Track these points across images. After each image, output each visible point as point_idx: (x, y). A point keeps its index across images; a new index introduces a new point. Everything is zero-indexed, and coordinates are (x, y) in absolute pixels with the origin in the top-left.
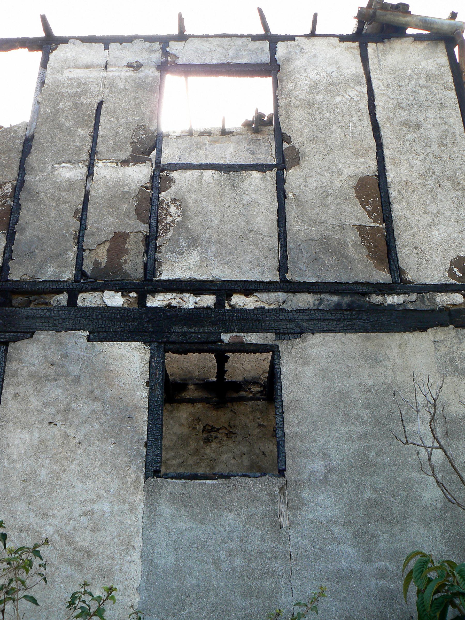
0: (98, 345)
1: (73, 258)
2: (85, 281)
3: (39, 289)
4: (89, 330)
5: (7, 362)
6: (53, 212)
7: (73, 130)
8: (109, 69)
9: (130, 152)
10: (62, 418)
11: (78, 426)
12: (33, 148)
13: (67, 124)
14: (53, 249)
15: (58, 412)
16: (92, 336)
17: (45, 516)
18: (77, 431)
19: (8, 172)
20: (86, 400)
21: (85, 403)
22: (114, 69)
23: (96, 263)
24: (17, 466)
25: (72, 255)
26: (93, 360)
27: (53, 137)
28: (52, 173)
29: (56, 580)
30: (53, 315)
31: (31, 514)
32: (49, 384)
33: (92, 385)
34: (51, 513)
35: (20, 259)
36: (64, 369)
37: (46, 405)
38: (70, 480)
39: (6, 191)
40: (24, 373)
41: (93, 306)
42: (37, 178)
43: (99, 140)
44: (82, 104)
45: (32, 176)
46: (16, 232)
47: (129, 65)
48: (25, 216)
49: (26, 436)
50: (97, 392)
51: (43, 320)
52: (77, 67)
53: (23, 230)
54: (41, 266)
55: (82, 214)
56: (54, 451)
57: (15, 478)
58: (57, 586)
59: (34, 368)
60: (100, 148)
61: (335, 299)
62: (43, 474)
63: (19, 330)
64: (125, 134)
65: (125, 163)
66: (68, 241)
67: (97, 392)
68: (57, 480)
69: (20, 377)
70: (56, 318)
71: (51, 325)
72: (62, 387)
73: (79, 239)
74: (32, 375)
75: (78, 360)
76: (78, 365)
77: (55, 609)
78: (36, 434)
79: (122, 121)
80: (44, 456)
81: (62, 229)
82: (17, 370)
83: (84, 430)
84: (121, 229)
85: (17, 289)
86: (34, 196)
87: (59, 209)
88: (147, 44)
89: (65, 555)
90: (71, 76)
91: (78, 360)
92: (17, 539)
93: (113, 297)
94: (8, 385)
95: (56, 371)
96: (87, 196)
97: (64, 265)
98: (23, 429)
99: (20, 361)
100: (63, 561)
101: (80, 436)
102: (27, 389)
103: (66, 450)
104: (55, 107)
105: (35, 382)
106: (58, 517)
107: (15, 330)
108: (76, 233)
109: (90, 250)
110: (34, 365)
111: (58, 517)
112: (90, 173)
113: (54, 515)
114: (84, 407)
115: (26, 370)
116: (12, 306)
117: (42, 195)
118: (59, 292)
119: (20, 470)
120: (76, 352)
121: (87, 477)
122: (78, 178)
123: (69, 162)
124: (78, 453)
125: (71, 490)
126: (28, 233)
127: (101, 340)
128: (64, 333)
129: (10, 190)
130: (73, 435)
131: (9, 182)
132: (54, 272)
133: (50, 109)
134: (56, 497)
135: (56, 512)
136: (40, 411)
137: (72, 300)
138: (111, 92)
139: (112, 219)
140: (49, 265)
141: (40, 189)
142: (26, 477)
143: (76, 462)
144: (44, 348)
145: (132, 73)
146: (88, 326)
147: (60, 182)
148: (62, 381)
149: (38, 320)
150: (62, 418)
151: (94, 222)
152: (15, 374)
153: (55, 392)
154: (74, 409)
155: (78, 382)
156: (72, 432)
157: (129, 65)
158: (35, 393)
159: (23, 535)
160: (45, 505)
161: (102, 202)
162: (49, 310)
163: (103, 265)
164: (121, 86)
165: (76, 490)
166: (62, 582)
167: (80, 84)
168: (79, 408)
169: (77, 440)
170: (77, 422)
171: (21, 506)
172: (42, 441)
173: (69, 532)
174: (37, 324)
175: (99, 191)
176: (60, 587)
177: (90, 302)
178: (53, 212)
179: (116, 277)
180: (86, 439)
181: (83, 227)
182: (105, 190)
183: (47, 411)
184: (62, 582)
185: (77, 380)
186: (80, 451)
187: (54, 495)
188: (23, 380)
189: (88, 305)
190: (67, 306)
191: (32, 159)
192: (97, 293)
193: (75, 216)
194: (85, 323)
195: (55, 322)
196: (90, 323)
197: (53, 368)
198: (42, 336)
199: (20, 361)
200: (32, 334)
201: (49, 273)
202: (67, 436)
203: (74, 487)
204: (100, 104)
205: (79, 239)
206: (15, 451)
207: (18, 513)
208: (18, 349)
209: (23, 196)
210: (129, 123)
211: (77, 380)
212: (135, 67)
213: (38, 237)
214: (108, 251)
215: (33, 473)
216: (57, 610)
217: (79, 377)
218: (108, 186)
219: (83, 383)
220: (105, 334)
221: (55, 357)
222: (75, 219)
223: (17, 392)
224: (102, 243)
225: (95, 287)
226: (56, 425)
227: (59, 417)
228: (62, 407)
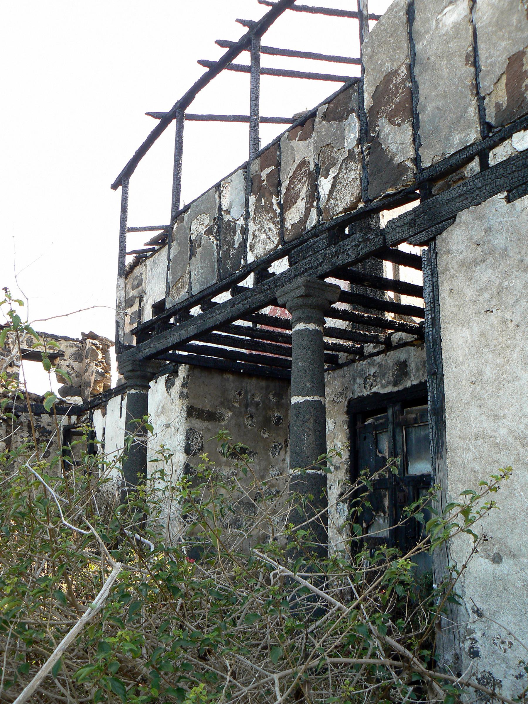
0: (518, 203)
1: (474, 113)
3: (451, 166)
4: (507, 189)
5: (438, 258)
6: (445, 72)
10: (497, 302)
12: (416, 11)
14: (454, 113)
16: (511, 195)
17: (497, 417)
18: (513, 312)
19: (399, 53)
20: (517, 273)
21: (517, 277)
23: (498, 106)
24: (464, 368)
25: (472, 112)
26: (517, 223)
29: (516, 488)
30: (469, 187)
31: (484, 418)
32: (478, 267)
33: (520, 253)
34: (501, 413)
35: (427, 141)
36: (490, 245)
37: (480, 292)
38: (514, 372)
39: (402, 74)
40: (454, 264)
41: (505, 159)
42: (425, 43)
45: (421, 44)
46: (419, 114)
49: (466, 333)
51: (462, 199)
53: (425, 107)
56: (495, 342)
57: (464, 381)
58: (517, 495)
59: (462, 256)
62: (489, 372)
63: (443, 219)
66: (466, 96)
68: (503, 374)
69: (452, 270)
70: (472, 190)
71: (470, 201)
72: (491, 267)
74: (462, 264)
75: (502, 229)
76: (503, 236)
77: (518, 520)
78: (475, 328)
80: (485, 350)
82: (448, 263)
83: (519, 309)
84: (515, 50)
85: (432, 175)
87: (451, 64)
89: (521, 459)
91: (502, 229)
92: (475, 448)
95: (485, 251)
97: (467, 126)
99: (448, 253)
100: (520, 466)
101: (517, 318)
103: (505, 338)
105: (466, 271)
106: (509, 416)
107: (439, 220)
108: (472, 83)
109: (489, 94)
110: (462, 252)
111: (509, 416)
113: (505, 415)
115: (455, 260)
116: (434, 196)
117: (432, 59)
118: (470, 159)
119: (467, 372)
120: (498, 220)
122: (462, 17)
124: (518, 338)
125: (517, 383)
126: (429, 109)
127: (520, 196)
128: (483, 204)
130: (509, 319)
131: (402, 64)
132: (460, 139)
134: (504, 394)
135: (506, 411)
140: (453, 134)
142: (473, 379)
143: (517, 349)
144: (468, 230)
146: (505, 185)
148: (490, 260)
149: (457, 200)
150: (497, 302)
151: (487, 58)
152: (447, 269)
153: (486, 274)
154: (506, 288)
155: (506, 255)
156: (508, 315)
158: (468, 282)
159: (480, 442)
160: (495, 406)
161: (490, 29)
162: (464, 185)
163: (505, 105)
165: (522, 382)
166: (522, 489)
168: (511, 285)
169: (514, 323)
170: (511, 302)
171: (474, 411)
172: (482, 334)
173: (522, 432)
174: (458, 205)
175: (485, 18)
176: (521, 495)
177: (502, 155)
178: (445, 72)
179: (521, 112)
180: (523, 319)
182: (490, 12)
183: (481, 299)
184: (522, 489)
185: (505, 253)
186: (519, 335)
187: (501, 392)
188: (454, 272)
189: (500, 160)
190: (481, 172)
194: (502, 182)
195: (473, 195)
196: (506, 180)
197: (480, 248)
198: (463, 217)
199: (448, 253)
201: (455, 143)
202: (505, 321)
203: (519, 379)
206: (460, 352)
207: (472, 420)
209: (417, 71)
213: (438, 108)
214: (506, 85)
215: (480, 373)
216: (521, 522)
217: (506, 249)
219: (511, 255)
220: (524, 186)
221: (478, 235)
222: (468, 67)
223: (451, 287)
224: (499, 80)
225: (503, 135)
226: (492, 311)
227: (494, 302)
228: (494, 289)
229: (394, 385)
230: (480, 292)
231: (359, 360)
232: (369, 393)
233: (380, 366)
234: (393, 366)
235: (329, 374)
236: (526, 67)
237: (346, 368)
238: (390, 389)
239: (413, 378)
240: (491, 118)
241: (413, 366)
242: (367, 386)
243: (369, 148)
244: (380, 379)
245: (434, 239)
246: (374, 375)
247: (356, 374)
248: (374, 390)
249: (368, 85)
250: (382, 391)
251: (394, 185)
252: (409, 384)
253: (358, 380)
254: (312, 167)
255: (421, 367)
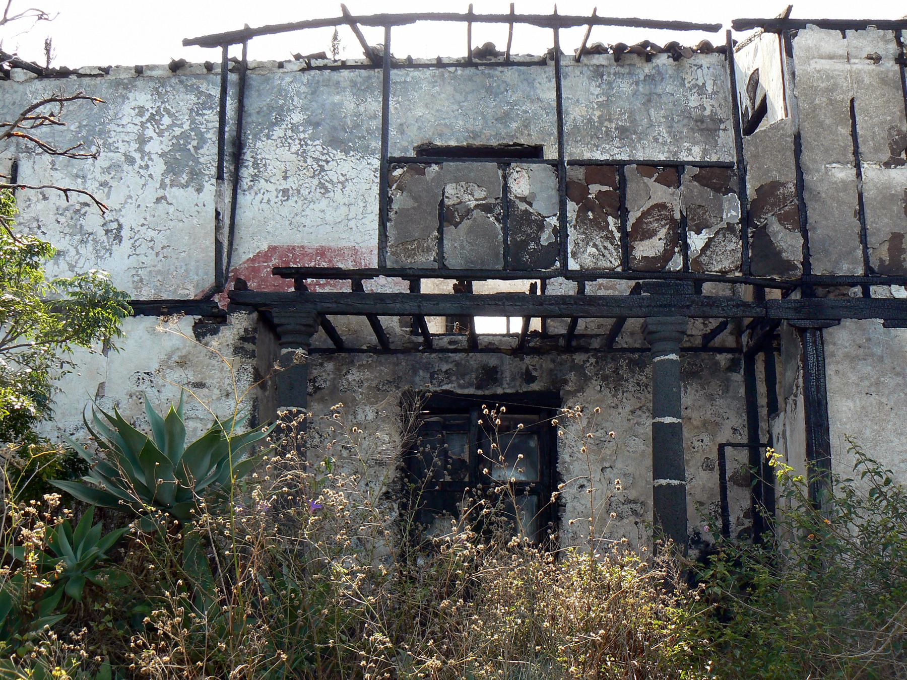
0: (892, 330)
2: (871, 277)
7: (834, 128)
8: (852, 61)
9: (889, 154)
11: (888, 396)
13: (827, 121)
15: (871, 385)
22: (856, 61)
23: (881, 260)
25: (860, 253)
27: (818, 135)
28: (826, 173)
32: (860, 362)
37: (861, 379)
40: (840, 353)
43: (860, 140)
44: (837, 101)
47: (869, 57)
48: (813, 215)
49: (851, 404)
50: (898, 369)
52: (821, 57)
53: (814, 229)
54: (837, 262)
55: (861, 214)
60: (862, 149)
61: (516, 324)
64: (881, 134)
65: (887, 165)
67: (898, 369)
73: (863, 236)
74: (846, 356)
79: (876, 120)
81: (847, 229)
84: (896, 230)
86: (816, 196)
88: (881, 32)
90: (818, 67)
93: (898, 291)
94: (830, 364)
95: (863, 353)
96: (860, 196)
98: (848, 398)
99: (835, 344)
102: (845, 367)
104: (812, 102)
112: (859, 175)
114: (890, 381)
115: (840, 351)
118: (853, 285)
121: (901, 434)
123: (839, 162)
126: (819, 231)
129: (793, 189)
133: (808, 104)
136: (857, 385)
137: (357, 287)
138: (859, 88)
139: (886, 220)
141: (820, 189)
143: (891, 423)
145: (873, 67)
147: (835, 183)
148: (870, 360)
151: (872, 222)
152: (833, 355)
153: (866, 369)
156: (884, 400)
157: (869, 57)
163: (887, 263)
164: (867, 80)
167: (829, 77)
172: (863, 407)
181: (864, 229)
183: (862, 384)
185: (881, 359)
187: (878, 448)
191: (805, 157)
192: (885, 287)
193: (855, 217)
197: (862, 349)
199: (835, 344)
200: (839, 320)
202: (881, 403)
204: (852, 101)
205: (863, 236)
208: (831, 334)
209: (806, 195)
210: (882, 123)
211: (881, 359)
212: (876, 59)
214: (888, 250)
218: (877, 188)
227: (873, 389)
229: (478, 388)
230: (861, 379)
231: (423, 352)
232: (438, 389)
233: (458, 364)
234: (477, 369)
235: (371, 356)
236: (904, 246)
237: (401, 356)
238: (471, 391)
239: (505, 386)
240: (874, 264)
241: (507, 374)
242: (434, 381)
243: (753, 232)
244: (457, 378)
245: (820, 329)
246: (446, 372)
247: (418, 366)
248: (445, 387)
249: (752, 178)
250: (459, 391)
251: (780, 274)
252: (499, 391)
253: (421, 373)
254: (677, 216)
255: (517, 377)
